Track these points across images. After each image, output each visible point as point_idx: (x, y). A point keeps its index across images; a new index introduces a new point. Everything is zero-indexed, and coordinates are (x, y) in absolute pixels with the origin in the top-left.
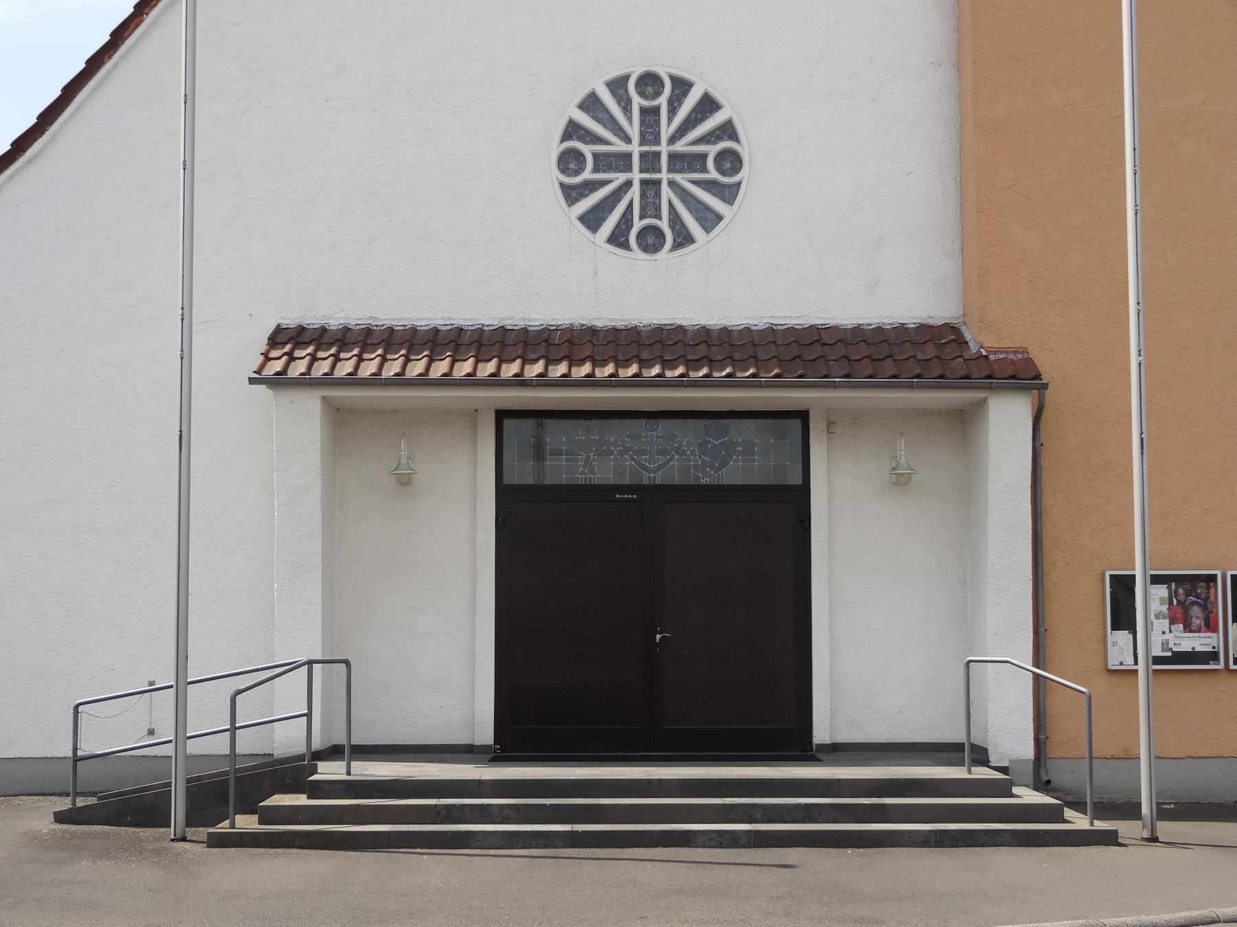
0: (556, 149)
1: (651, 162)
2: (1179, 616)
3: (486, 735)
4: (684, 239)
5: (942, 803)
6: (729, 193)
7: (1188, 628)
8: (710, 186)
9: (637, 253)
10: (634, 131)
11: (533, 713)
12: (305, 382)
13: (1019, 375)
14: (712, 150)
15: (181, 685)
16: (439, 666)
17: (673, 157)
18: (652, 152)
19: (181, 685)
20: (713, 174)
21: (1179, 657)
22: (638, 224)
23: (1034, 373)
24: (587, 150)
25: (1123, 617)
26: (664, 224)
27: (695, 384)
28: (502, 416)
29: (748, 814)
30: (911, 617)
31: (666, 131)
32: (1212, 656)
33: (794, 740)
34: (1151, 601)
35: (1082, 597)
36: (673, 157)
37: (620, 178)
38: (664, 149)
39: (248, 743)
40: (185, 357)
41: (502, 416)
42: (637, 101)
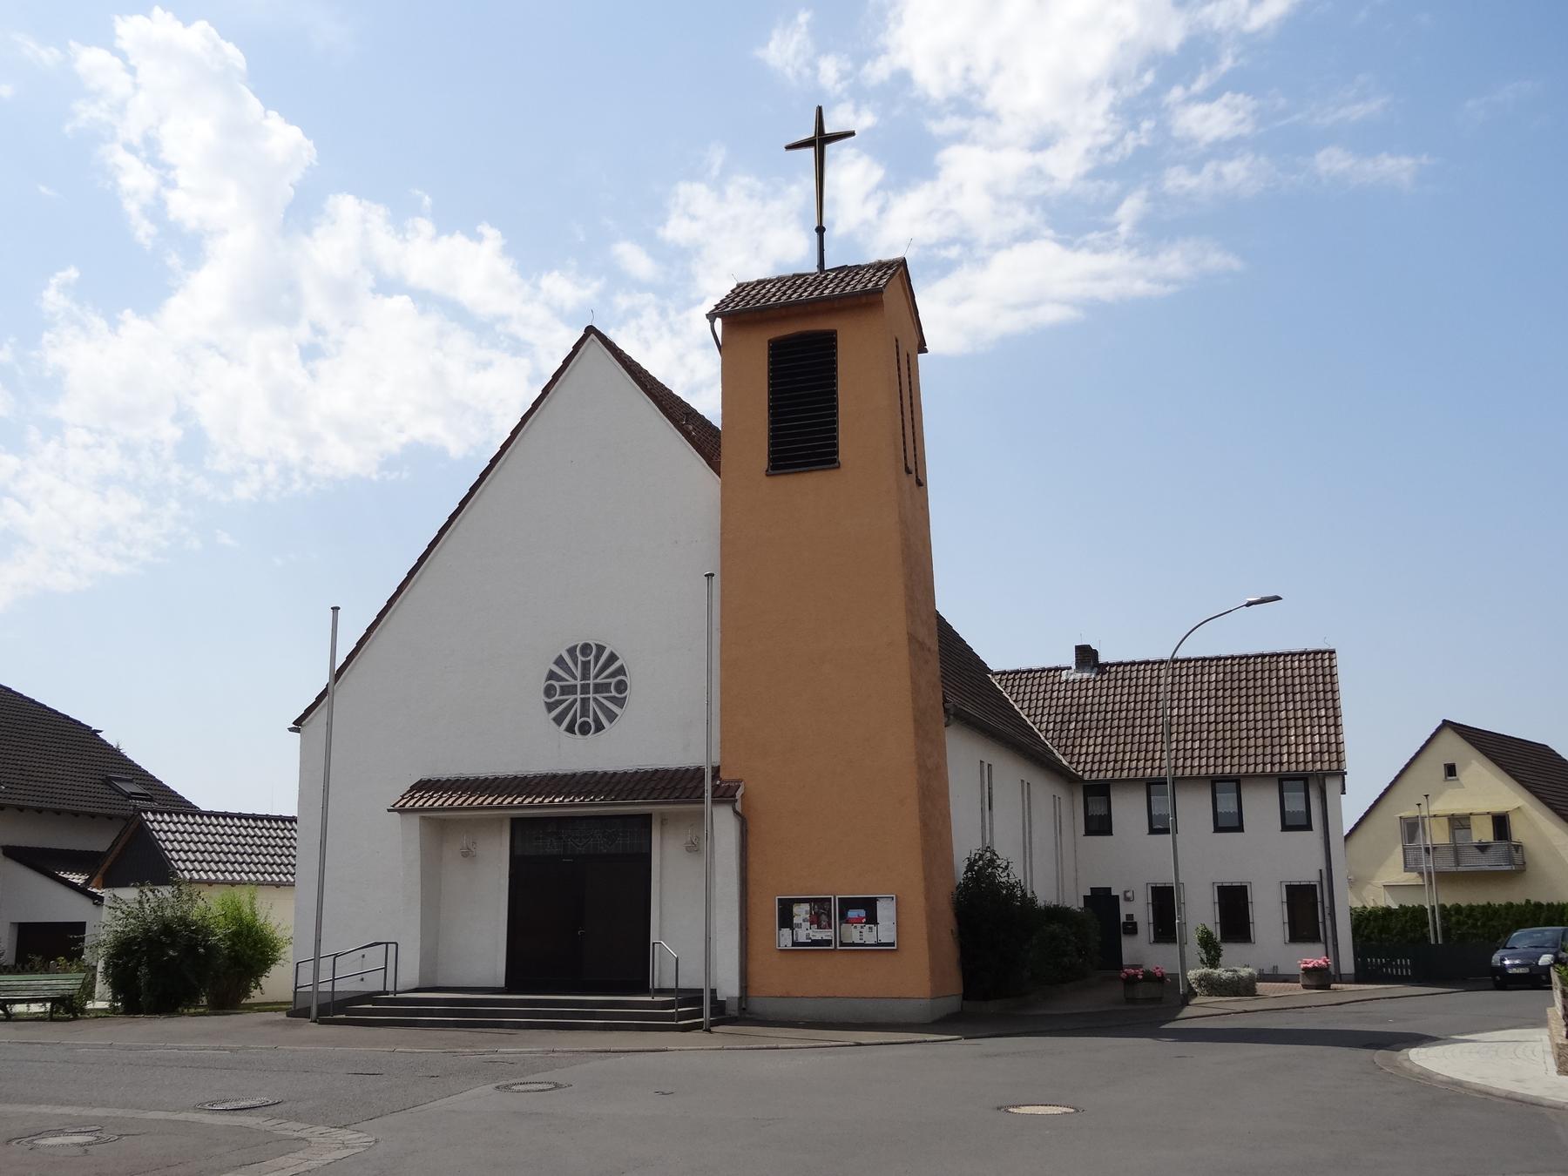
0: (543, 685)
1: (585, 689)
2: (815, 920)
3: (501, 983)
4: (600, 727)
5: (695, 1010)
6: (620, 703)
7: (819, 927)
8: (612, 699)
9: (578, 735)
10: (578, 674)
11: (526, 966)
12: (413, 810)
13: (724, 795)
14: (614, 681)
15: (317, 958)
16: (482, 952)
17: (596, 685)
18: (587, 685)
19: (317, 958)
20: (614, 693)
21: (815, 943)
22: (579, 721)
23: (1297, 756)
24: (557, 684)
25: (786, 920)
26: (590, 720)
27: (516, 807)
28: (515, 822)
29: (407, 1013)
30: (694, 919)
31: (593, 672)
32: (828, 943)
33: (642, 986)
34: (801, 912)
35: (764, 909)
36: (596, 685)
37: (572, 698)
38: (591, 682)
39: (341, 986)
40: (325, 808)
41: (515, 822)
42: (580, 658)
